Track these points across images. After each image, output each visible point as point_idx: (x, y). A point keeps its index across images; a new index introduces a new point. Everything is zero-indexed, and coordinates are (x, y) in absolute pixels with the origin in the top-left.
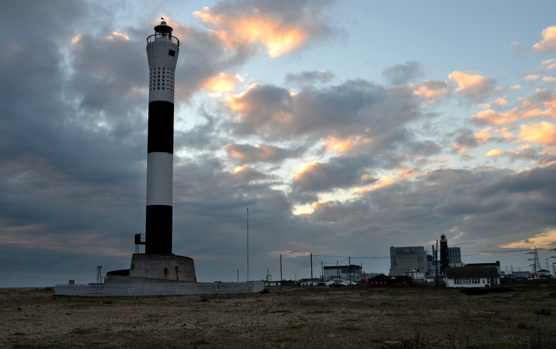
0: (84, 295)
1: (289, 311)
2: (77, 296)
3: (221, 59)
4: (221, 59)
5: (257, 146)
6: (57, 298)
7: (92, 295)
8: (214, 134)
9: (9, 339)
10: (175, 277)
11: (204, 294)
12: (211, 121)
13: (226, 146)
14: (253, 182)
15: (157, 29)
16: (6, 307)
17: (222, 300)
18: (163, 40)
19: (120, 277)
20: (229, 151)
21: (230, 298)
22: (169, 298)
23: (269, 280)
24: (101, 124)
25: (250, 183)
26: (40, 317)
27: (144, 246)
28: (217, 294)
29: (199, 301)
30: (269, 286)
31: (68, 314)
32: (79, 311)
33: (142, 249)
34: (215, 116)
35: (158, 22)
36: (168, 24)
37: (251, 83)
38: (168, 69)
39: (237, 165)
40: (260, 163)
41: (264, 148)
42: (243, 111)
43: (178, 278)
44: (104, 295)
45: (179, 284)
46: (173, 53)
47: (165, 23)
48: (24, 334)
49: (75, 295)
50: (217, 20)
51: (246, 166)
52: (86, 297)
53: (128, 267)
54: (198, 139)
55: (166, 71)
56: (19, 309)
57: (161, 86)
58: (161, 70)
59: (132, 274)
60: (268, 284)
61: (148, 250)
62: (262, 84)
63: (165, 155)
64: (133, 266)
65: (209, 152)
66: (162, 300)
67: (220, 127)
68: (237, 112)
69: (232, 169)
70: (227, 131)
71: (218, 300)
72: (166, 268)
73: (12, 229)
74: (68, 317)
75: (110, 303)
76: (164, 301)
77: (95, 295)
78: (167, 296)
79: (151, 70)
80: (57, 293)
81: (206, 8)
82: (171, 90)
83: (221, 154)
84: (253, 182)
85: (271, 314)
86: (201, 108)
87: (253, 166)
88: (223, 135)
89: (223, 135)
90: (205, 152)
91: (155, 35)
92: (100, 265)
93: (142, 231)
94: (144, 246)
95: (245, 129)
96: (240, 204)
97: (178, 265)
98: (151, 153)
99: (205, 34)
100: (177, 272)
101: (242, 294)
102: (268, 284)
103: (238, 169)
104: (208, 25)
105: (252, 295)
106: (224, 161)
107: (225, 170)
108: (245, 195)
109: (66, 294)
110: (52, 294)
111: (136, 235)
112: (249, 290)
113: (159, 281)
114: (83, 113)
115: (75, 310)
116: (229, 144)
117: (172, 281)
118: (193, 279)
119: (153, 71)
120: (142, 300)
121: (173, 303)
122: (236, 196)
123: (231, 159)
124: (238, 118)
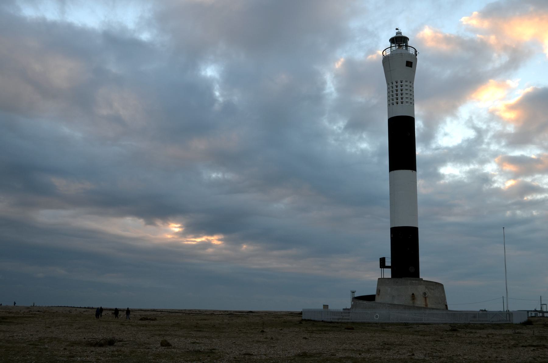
0: (329, 320)
1: (544, 345)
2: (322, 321)
3: (490, 67)
4: (490, 67)
5: (533, 156)
6: (304, 322)
7: (337, 321)
8: (484, 146)
9: (235, 358)
10: (424, 303)
11: (453, 324)
12: (480, 133)
13: (496, 159)
14: (528, 198)
15: (392, 40)
16: (252, 329)
17: (473, 331)
18: (400, 51)
19: (365, 302)
20: (500, 164)
21: (483, 329)
22: (415, 326)
23: (545, 310)
24: (364, 145)
25: (525, 198)
26: (277, 339)
27: (390, 270)
28: (469, 324)
29: (447, 331)
30: (543, 316)
31: (305, 338)
32: (318, 336)
33: (388, 274)
34: (484, 127)
35: (393, 34)
36: (404, 34)
37: (528, 86)
38: (406, 81)
39: (509, 179)
40: (537, 176)
41: (541, 158)
42: (516, 120)
43: (426, 305)
44: (349, 321)
45: (427, 311)
46: (410, 64)
47: (400, 33)
48: (252, 355)
49: (321, 320)
50: (486, 24)
51: (521, 179)
52: (331, 322)
53: (374, 292)
54: (464, 153)
55: (404, 83)
56: (263, 331)
57: (400, 100)
58: (399, 84)
59: (378, 300)
60: (541, 315)
61: (394, 275)
62: (539, 87)
63: (409, 171)
64: (379, 291)
65: (477, 166)
66: (408, 328)
67: (490, 139)
68: (509, 121)
69: (504, 184)
70: (499, 143)
71: (469, 330)
72: (413, 294)
73: (275, 253)
74: (304, 341)
75: (353, 329)
76: (410, 329)
77: (340, 320)
78: (414, 324)
79: (388, 84)
80: (304, 317)
81: (475, 13)
82: (411, 103)
83: (490, 168)
84: (528, 198)
85: (522, 348)
86: (468, 120)
87: (528, 180)
88: (494, 147)
89: (494, 147)
90: (472, 167)
91: (391, 47)
92: (353, 290)
93: (387, 253)
94: (390, 270)
95: (520, 139)
96: (514, 222)
97: (427, 290)
98: (392, 172)
99: (472, 41)
100: (426, 298)
101: (498, 325)
102: (541, 315)
103: (511, 183)
104: (474, 30)
105: (510, 326)
106: (494, 175)
107: (496, 185)
108: (518, 212)
109: (312, 319)
110: (300, 319)
111: (380, 259)
112: (509, 321)
113: (406, 307)
114: (347, 136)
115: (314, 335)
116: (501, 156)
117: (419, 308)
118: (444, 307)
119: (391, 85)
120: (387, 327)
121: (418, 332)
122: (508, 213)
123: (502, 173)
124: (511, 129)
